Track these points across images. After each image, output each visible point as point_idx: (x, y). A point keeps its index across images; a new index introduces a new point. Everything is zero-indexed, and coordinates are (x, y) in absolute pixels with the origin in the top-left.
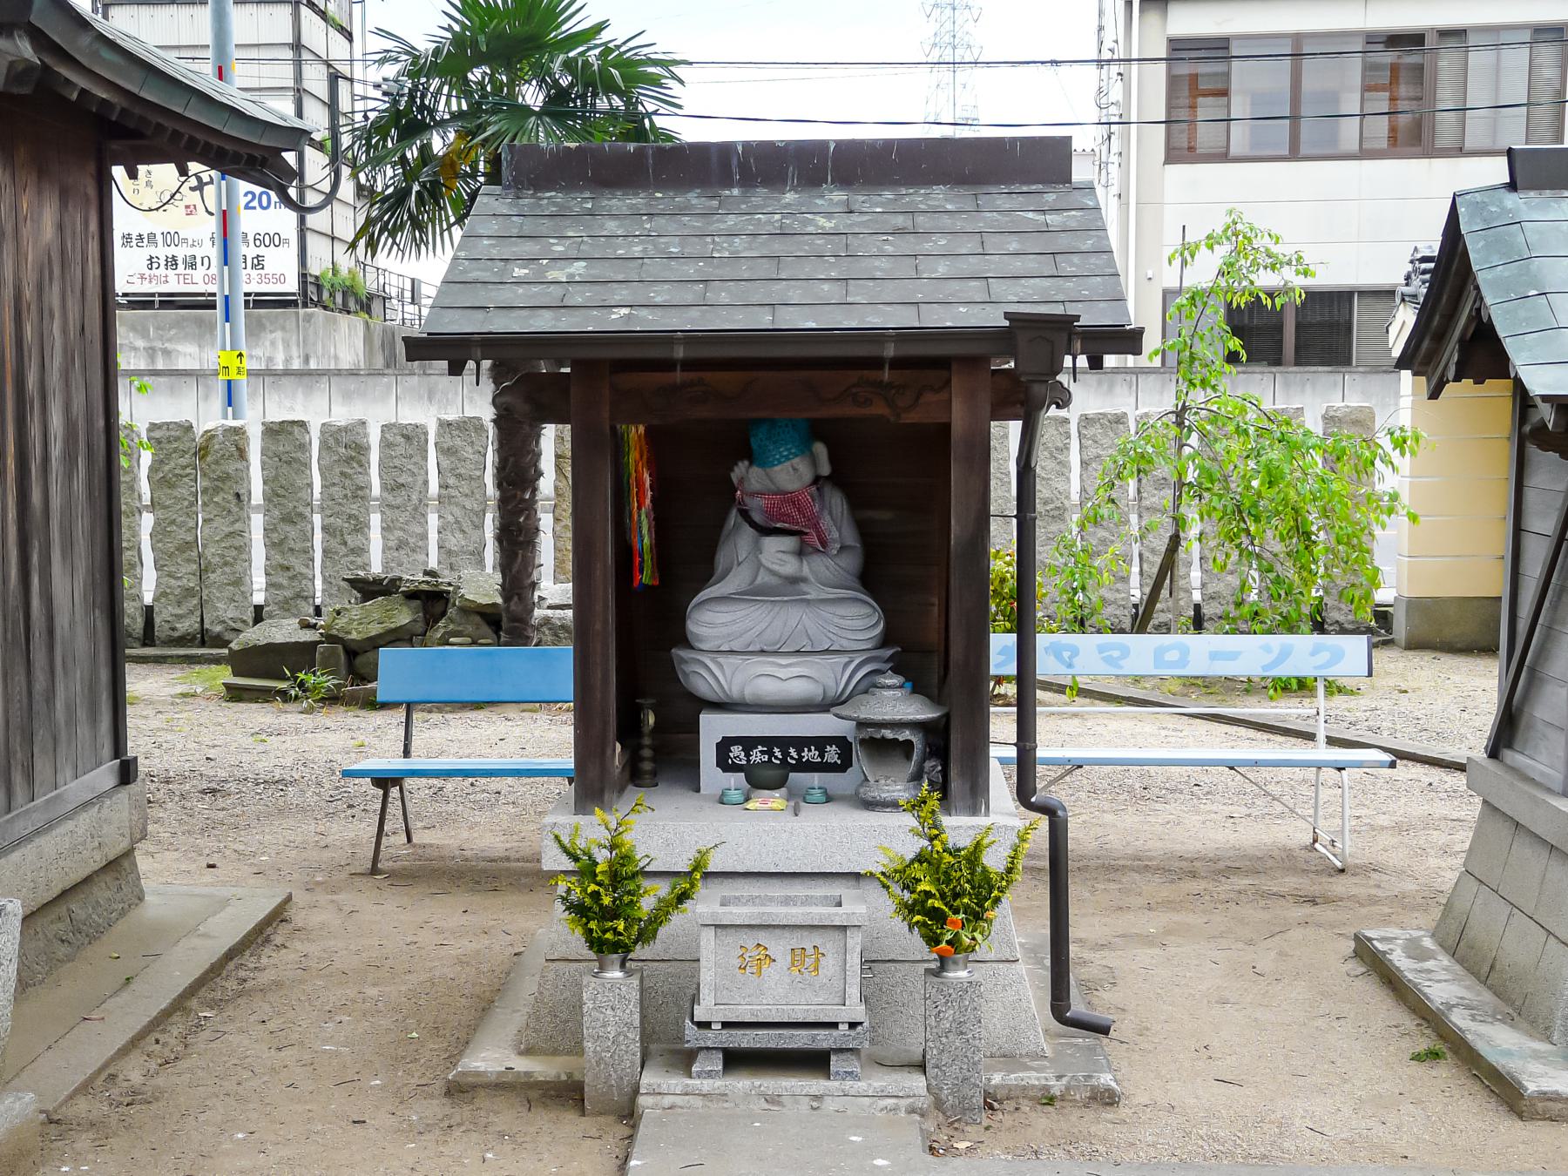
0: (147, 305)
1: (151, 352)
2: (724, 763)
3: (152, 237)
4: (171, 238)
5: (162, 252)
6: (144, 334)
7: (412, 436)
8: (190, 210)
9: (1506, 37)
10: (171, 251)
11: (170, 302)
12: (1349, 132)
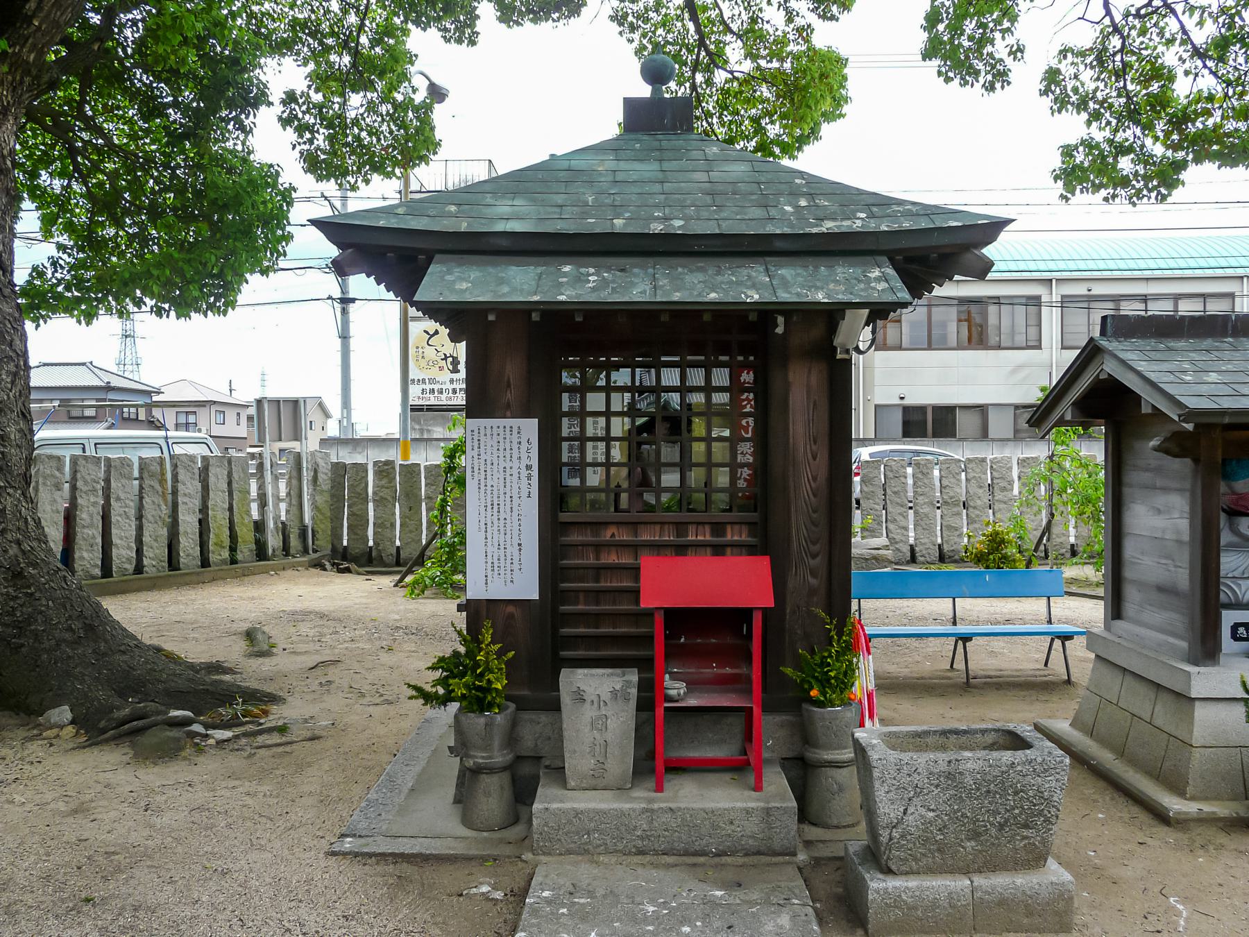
0: (421, 410)
1: (422, 431)
2: (1235, 637)
3: (424, 380)
4: (432, 381)
5: (428, 387)
6: (419, 423)
7: (362, 468)
8: (441, 369)
9: (1016, 301)
10: (432, 386)
11: (431, 409)
12: (953, 339)
